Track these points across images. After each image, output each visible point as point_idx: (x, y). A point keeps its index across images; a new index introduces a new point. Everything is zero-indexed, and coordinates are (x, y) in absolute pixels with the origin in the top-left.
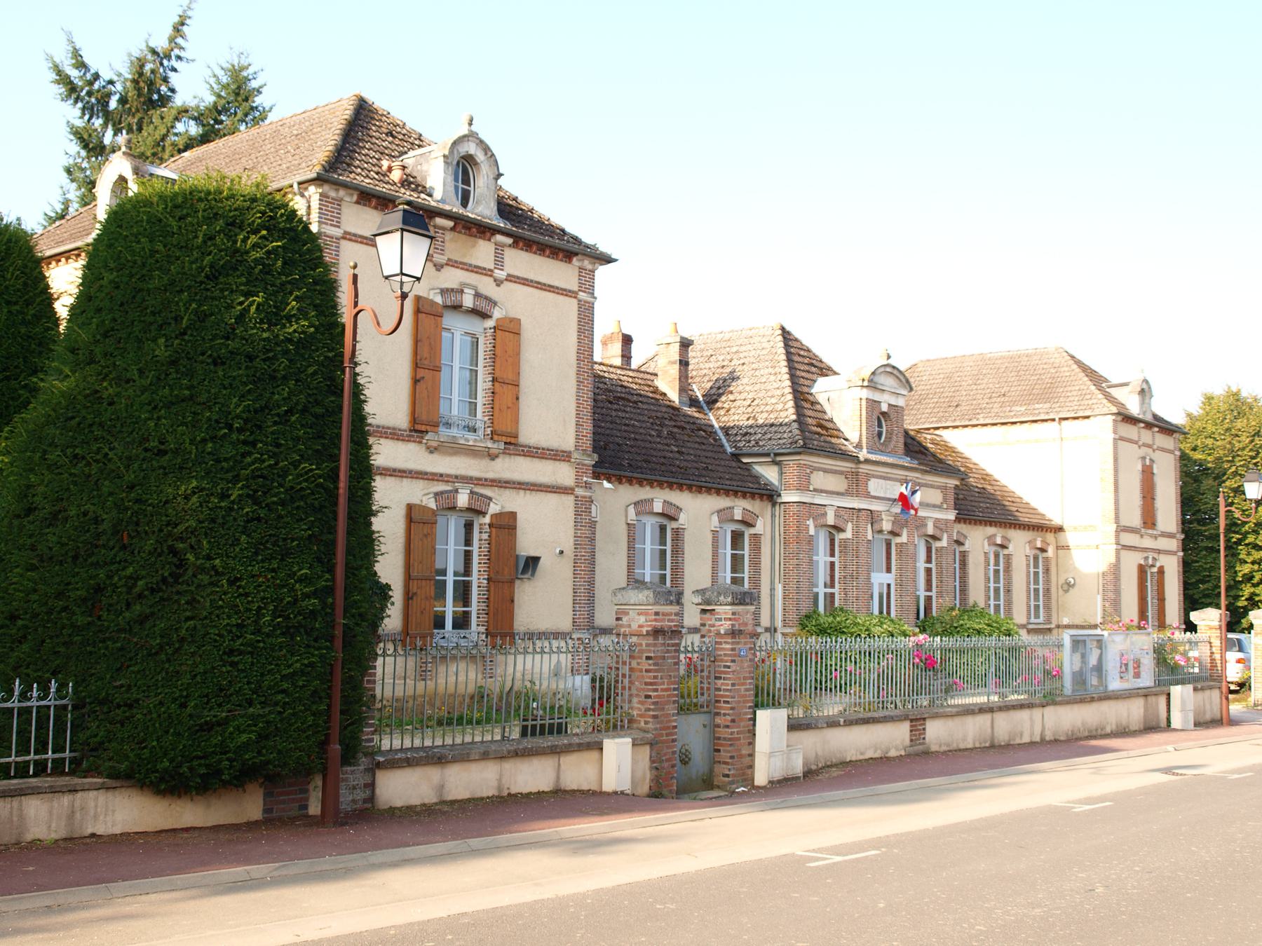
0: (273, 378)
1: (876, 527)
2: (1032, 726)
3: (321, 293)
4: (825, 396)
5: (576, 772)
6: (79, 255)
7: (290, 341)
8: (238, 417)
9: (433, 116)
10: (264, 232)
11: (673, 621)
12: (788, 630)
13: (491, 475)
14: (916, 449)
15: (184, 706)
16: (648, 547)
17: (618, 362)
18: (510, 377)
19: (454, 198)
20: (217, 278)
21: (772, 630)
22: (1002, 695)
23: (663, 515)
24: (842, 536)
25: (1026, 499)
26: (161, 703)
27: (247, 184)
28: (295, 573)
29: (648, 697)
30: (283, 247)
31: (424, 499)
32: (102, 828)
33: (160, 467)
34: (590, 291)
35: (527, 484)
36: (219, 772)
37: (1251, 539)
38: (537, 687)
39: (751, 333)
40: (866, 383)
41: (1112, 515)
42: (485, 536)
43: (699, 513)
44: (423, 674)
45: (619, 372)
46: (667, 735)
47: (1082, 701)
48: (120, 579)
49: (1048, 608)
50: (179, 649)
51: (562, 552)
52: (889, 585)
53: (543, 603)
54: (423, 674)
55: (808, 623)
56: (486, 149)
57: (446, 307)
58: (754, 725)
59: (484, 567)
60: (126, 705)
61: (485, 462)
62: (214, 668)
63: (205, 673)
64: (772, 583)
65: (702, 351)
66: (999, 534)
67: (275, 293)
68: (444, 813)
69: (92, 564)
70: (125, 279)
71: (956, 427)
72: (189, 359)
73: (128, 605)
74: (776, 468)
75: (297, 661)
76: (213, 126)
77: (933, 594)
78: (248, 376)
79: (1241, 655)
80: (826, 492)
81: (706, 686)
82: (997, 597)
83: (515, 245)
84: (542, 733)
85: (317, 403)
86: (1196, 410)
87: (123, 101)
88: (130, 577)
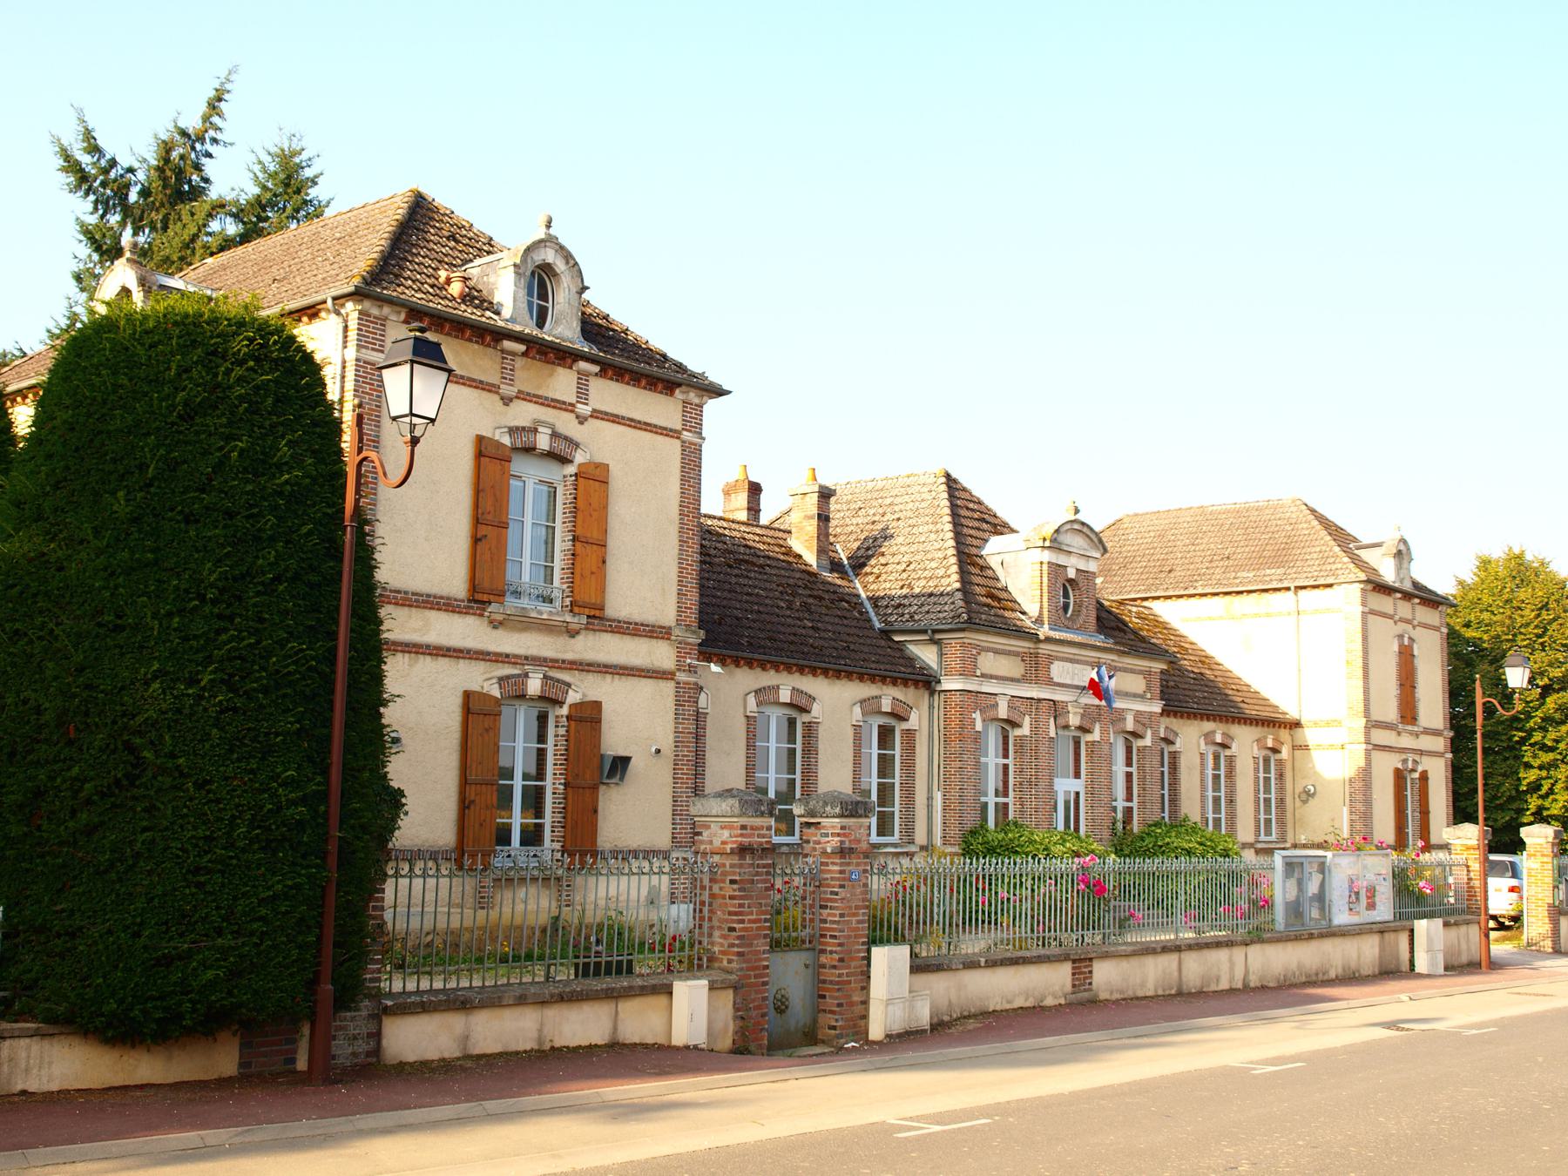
0: (257, 539)
1: (1061, 721)
2: (1232, 969)
4: (999, 559)
5: (638, 1021)
6: (25, 397)
8: (212, 585)
12: (949, 849)
13: (569, 656)
15: (137, 935)
16: (773, 745)
17: (743, 516)
18: (594, 535)
19: (527, 317)
20: (192, 418)
23: (790, 705)
24: (1018, 732)
25: (1255, 686)
26: (110, 932)
29: (732, 929)
30: (276, 381)
31: (486, 685)
32: (33, 1086)
34: (697, 429)
35: (615, 666)
37: (1537, 737)
39: (908, 481)
40: (1047, 544)
41: (1361, 707)
42: (562, 731)
43: (837, 704)
44: (483, 902)
45: (743, 528)
47: (1297, 938)
48: (64, 781)
49: (1282, 823)
50: (134, 865)
51: (658, 751)
52: (1077, 794)
53: (634, 814)
54: (483, 902)
55: (974, 843)
56: (568, 257)
57: (515, 449)
58: (869, 965)
60: (67, 934)
64: (930, 790)
65: (848, 502)
66: (1219, 731)
67: (263, 437)
70: (82, 419)
71: (1169, 597)
73: (73, 813)
74: (934, 649)
75: (279, 882)
77: (1134, 804)
78: (225, 536)
79: (1514, 882)
80: (996, 677)
81: (808, 917)
83: (603, 373)
84: (597, 973)
87: (145, 193)
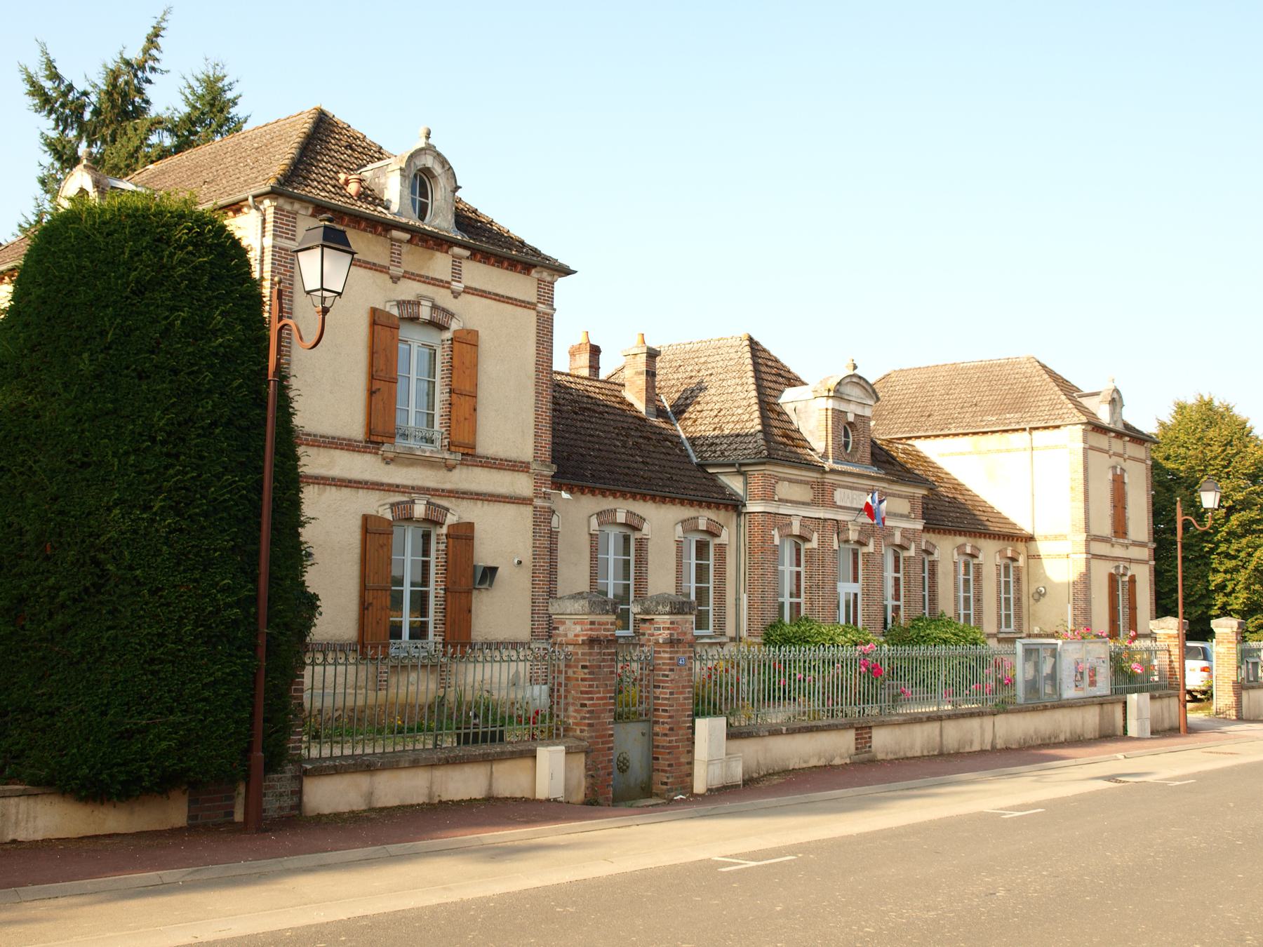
0: (197, 391)
1: (843, 537)
3: (248, 308)
4: (792, 406)
5: (508, 779)
8: (161, 430)
9: (389, 127)
13: (448, 486)
14: (884, 459)
15: (104, 714)
16: (408, 558)
17: (585, 372)
18: (467, 388)
20: (143, 294)
21: (737, 639)
23: (625, 525)
24: (808, 545)
26: (82, 711)
27: (174, 203)
28: (217, 584)
30: (211, 263)
31: (380, 510)
33: (83, 480)
36: (140, 779)
37: (1223, 548)
40: (831, 394)
42: (442, 547)
43: (663, 523)
44: (380, 684)
45: (586, 382)
47: (1035, 709)
48: (43, 590)
49: (1019, 617)
50: (101, 657)
51: (520, 562)
52: (856, 595)
53: (501, 613)
54: (380, 684)
55: (773, 634)
56: (444, 162)
57: (402, 319)
58: (693, 733)
59: (441, 578)
60: (47, 713)
61: (442, 473)
62: (134, 676)
63: (126, 681)
64: (738, 592)
65: (671, 361)
66: (968, 544)
69: (15, 575)
71: (929, 437)
72: (114, 373)
73: (51, 615)
74: (741, 479)
76: (187, 137)
78: (172, 389)
79: (1205, 664)
80: (791, 502)
81: (644, 695)
82: (967, 607)
83: (473, 257)
84: (475, 741)
85: (242, 415)
87: (97, 112)
88: (52, 588)
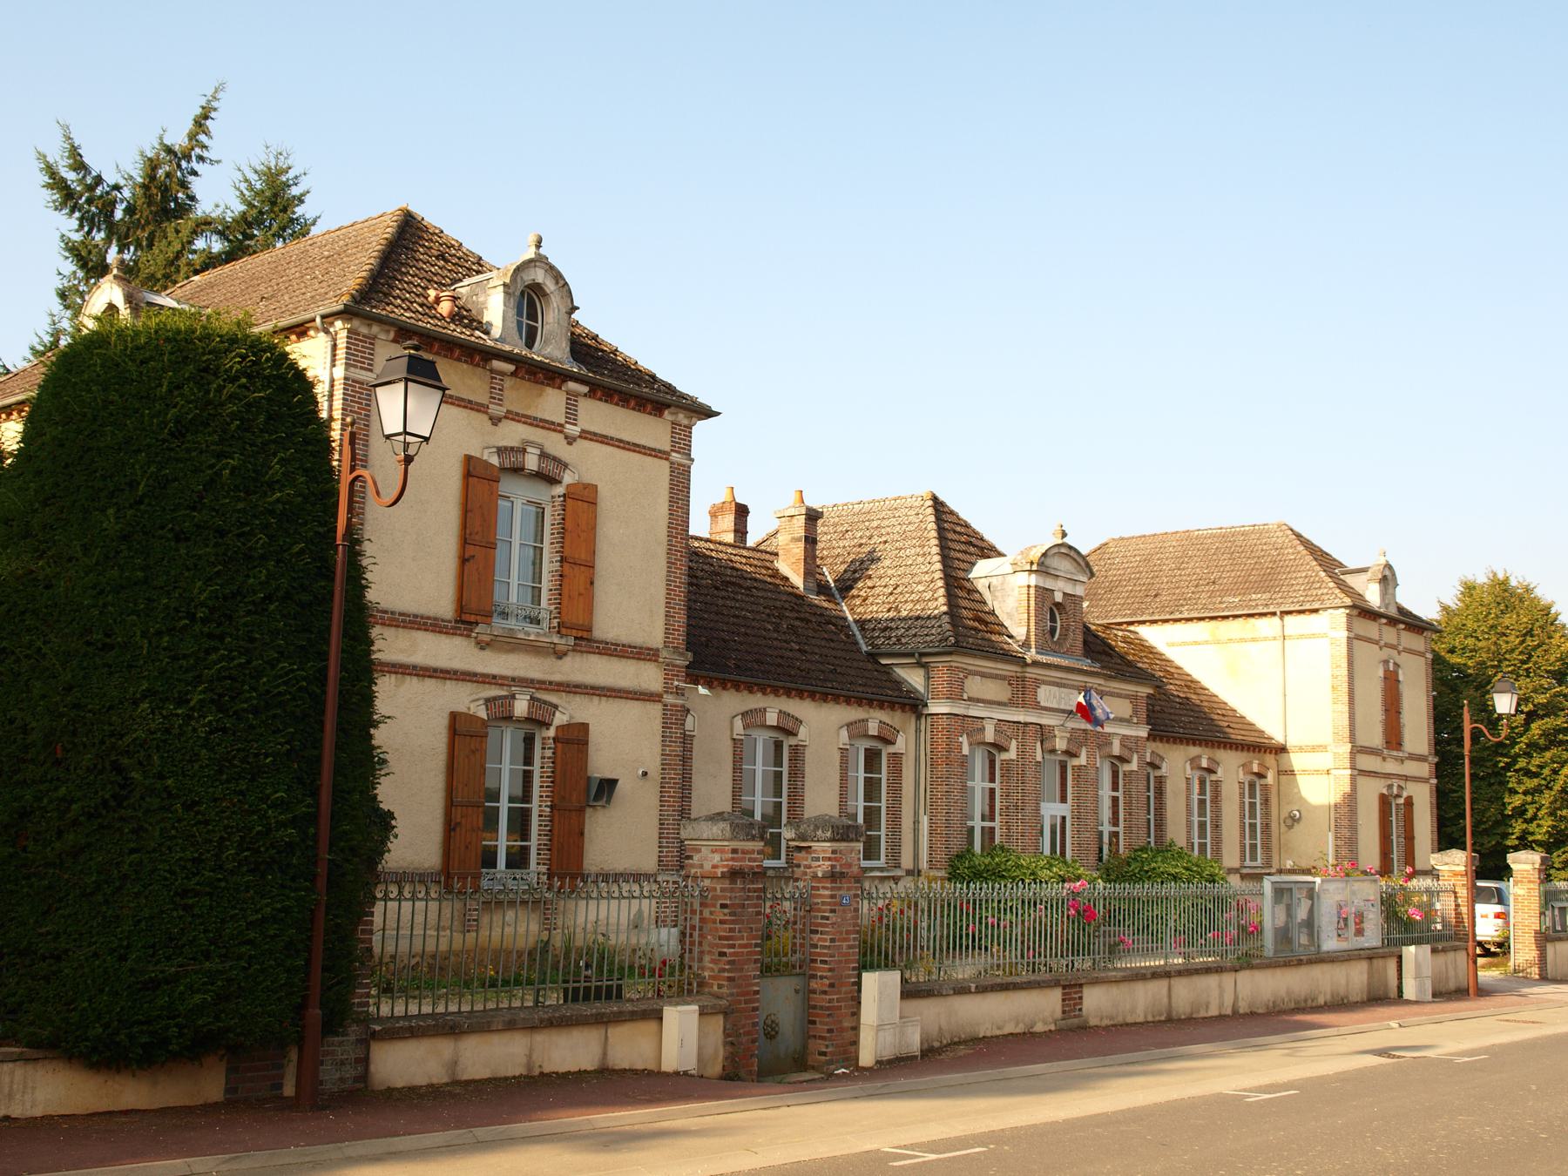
1: (1048, 745)
2: (1221, 996)
4: (985, 582)
5: (628, 1047)
7: (272, 512)
8: (202, 604)
10: (244, 380)
11: (755, 860)
13: (557, 678)
14: (1100, 649)
15: (123, 958)
17: (729, 538)
18: (583, 556)
19: (517, 337)
20: (183, 436)
21: (914, 872)
22: (1186, 956)
23: (777, 728)
24: (1004, 756)
26: (96, 955)
30: (268, 399)
35: (603, 688)
37: (1522, 763)
38: (613, 942)
40: (1035, 567)
42: (549, 753)
43: (824, 726)
45: (730, 550)
46: (746, 1002)
47: (1287, 964)
48: (51, 802)
49: (1267, 848)
50: (119, 889)
51: (645, 774)
52: (1064, 818)
53: (622, 837)
54: (467, 924)
55: (960, 867)
56: (558, 277)
57: (503, 469)
58: (859, 991)
64: (916, 814)
65: (835, 525)
68: (452, 1095)
71: (1155, 622)
72: (145, 533)
73: (60, 833)
74: (921, 672)
81: (798, 941)
83: (591, 394)
84: (586, 998)
86: (1452, 601)
87: (130, 210)
